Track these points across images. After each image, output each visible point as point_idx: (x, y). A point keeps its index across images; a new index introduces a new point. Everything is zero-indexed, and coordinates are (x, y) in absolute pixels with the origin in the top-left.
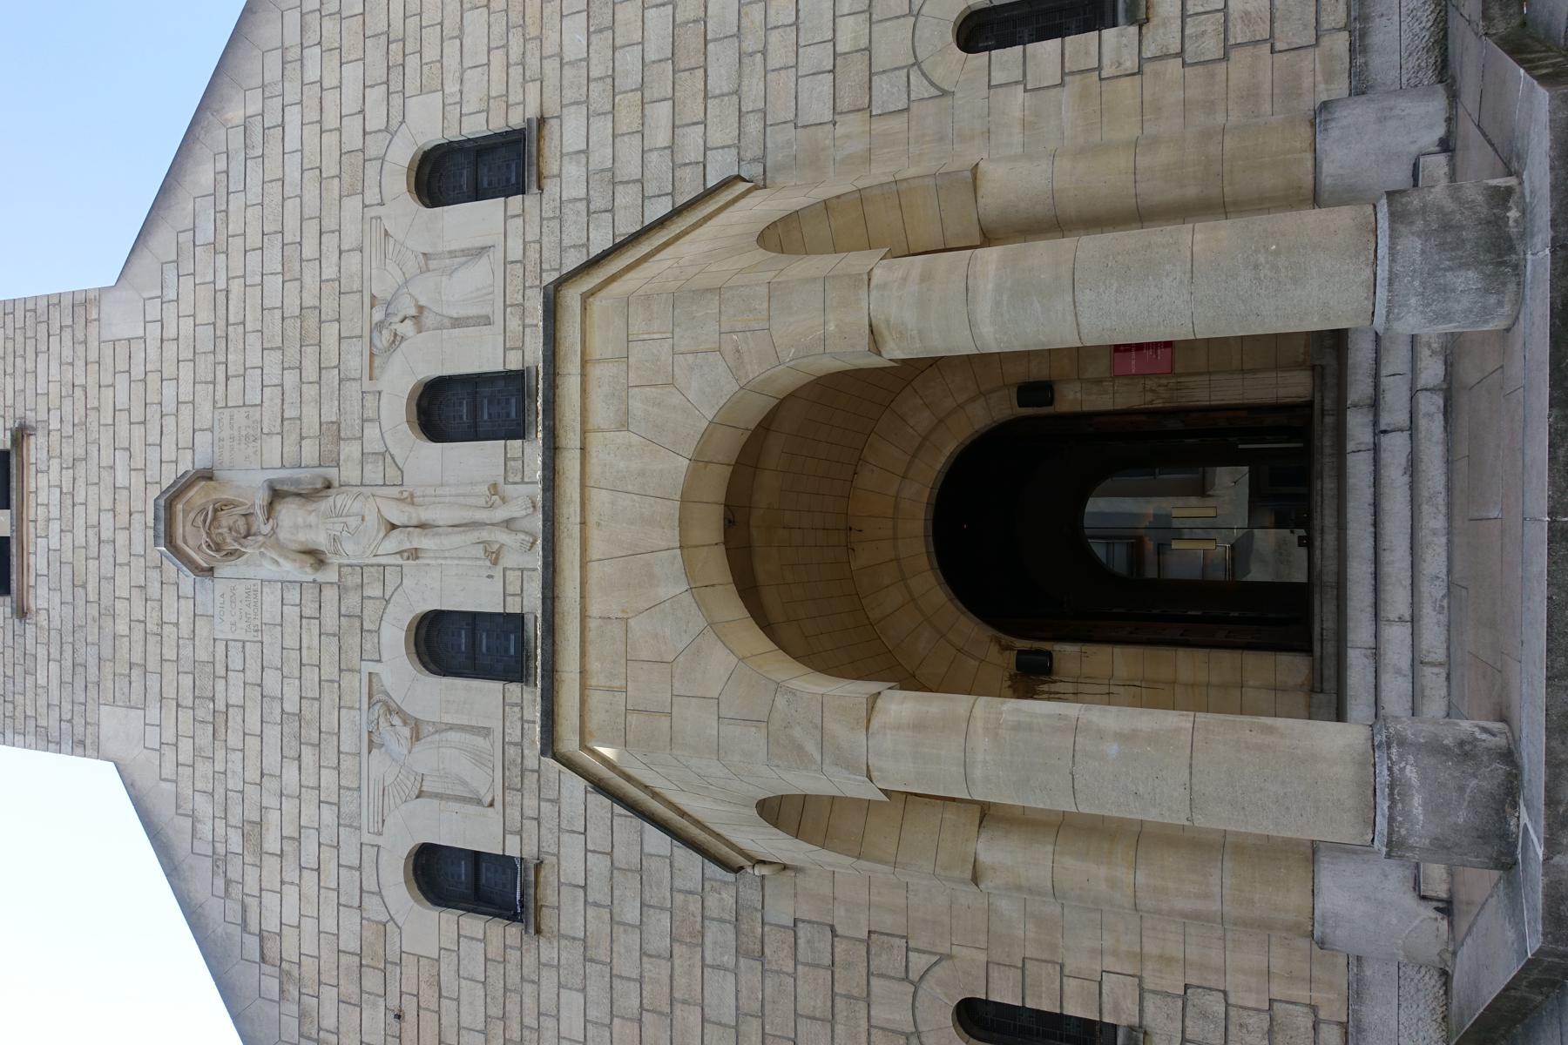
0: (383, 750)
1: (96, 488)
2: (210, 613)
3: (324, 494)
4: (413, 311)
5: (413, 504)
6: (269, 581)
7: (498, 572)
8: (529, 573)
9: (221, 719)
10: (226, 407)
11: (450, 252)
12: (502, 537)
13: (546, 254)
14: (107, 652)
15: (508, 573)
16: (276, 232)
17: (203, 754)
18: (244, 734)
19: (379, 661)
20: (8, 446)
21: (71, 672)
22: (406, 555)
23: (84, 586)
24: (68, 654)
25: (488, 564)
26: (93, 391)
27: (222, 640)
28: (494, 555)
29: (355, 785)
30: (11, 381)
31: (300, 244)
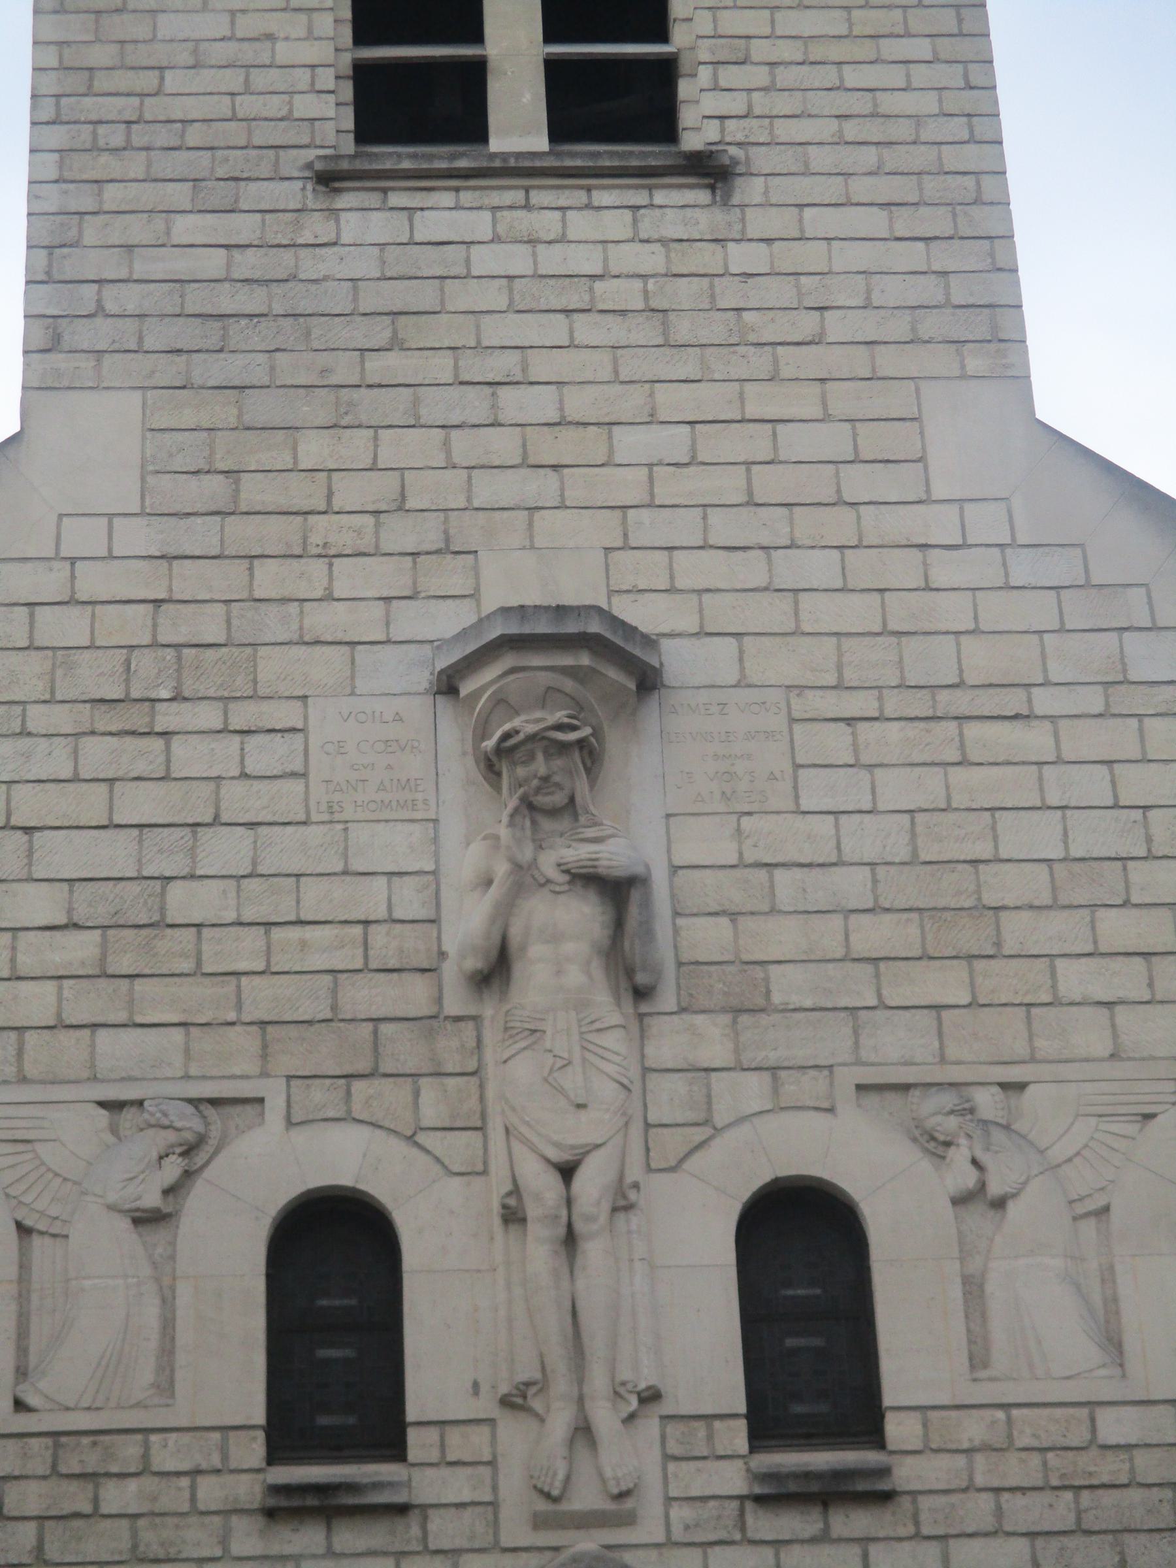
0: (111, 1139)
1: (606, 374)
2: (361, 686)
3: (624, 984)
4: (995, 1188)
5: (615, 1209)
6: (435, 840)
7: (485, 1406)
8: (488, 1481)
9: (136, 718)
10: (793, 720)
11: (1111, 1268)
12: (560, 1422)
13: (1108, 1498)
14: (262, 408)
15: (485, 1430)
16: (1149, 840)
17: (59, 672)
18: (111, 781)
19: (290, 1123)
20: (691, 142)
21: (209, 310)
22: (512, 1202)
23: (396, 344)
24: (251, 300)
25: (504, 1389)
26: (810, 361)
27: (306, 718)
28: (519, 1401)
29: (30, 1070)
30: (826, 136)
31: (1126, 904)
